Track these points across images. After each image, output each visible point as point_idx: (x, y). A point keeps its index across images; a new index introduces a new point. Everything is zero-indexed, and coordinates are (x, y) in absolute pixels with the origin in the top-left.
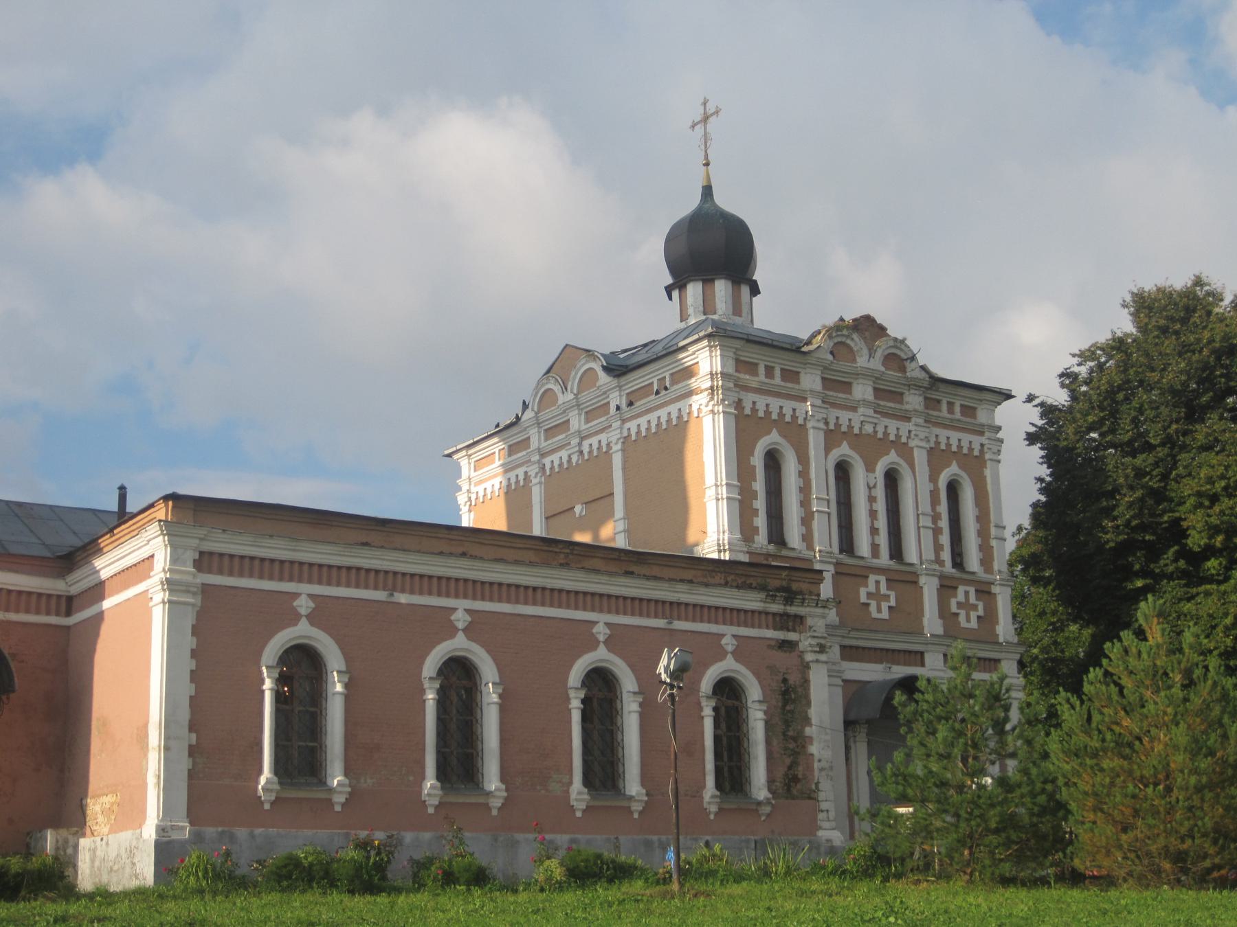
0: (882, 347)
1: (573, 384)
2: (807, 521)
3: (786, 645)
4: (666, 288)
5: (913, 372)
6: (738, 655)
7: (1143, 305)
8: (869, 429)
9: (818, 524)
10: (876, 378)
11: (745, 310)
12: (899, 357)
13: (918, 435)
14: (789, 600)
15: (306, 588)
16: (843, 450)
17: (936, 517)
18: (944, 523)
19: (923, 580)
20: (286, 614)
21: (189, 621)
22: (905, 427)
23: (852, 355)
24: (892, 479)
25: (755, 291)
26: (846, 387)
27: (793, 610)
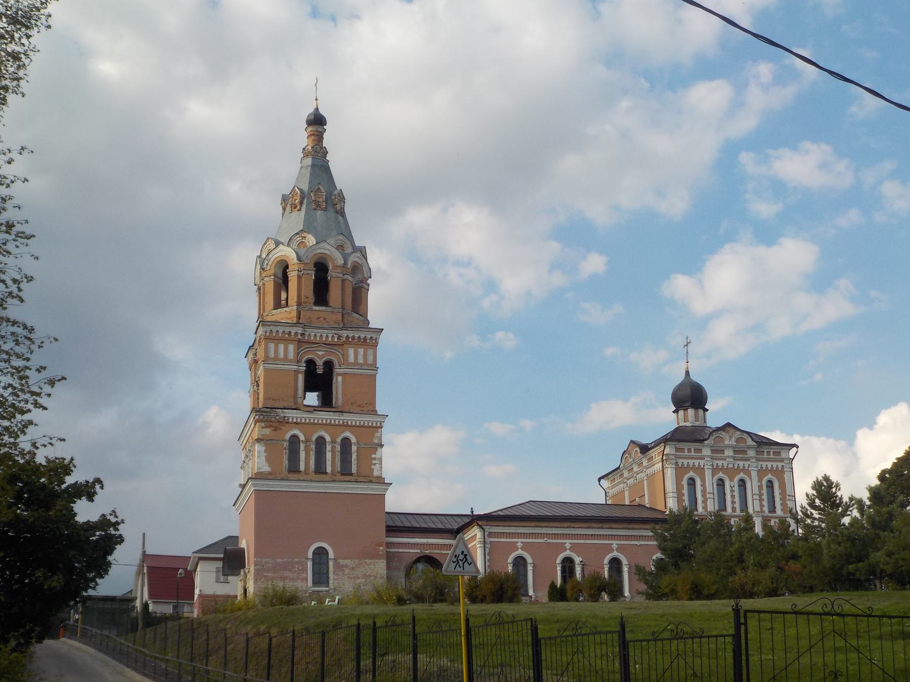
4: (632, 442)
8: (731, 466)
16: (720, 475)
17: (760, 495)
19: (755, 519)
20: (514, 547)
22: (747, 464)
23: (722, 440)
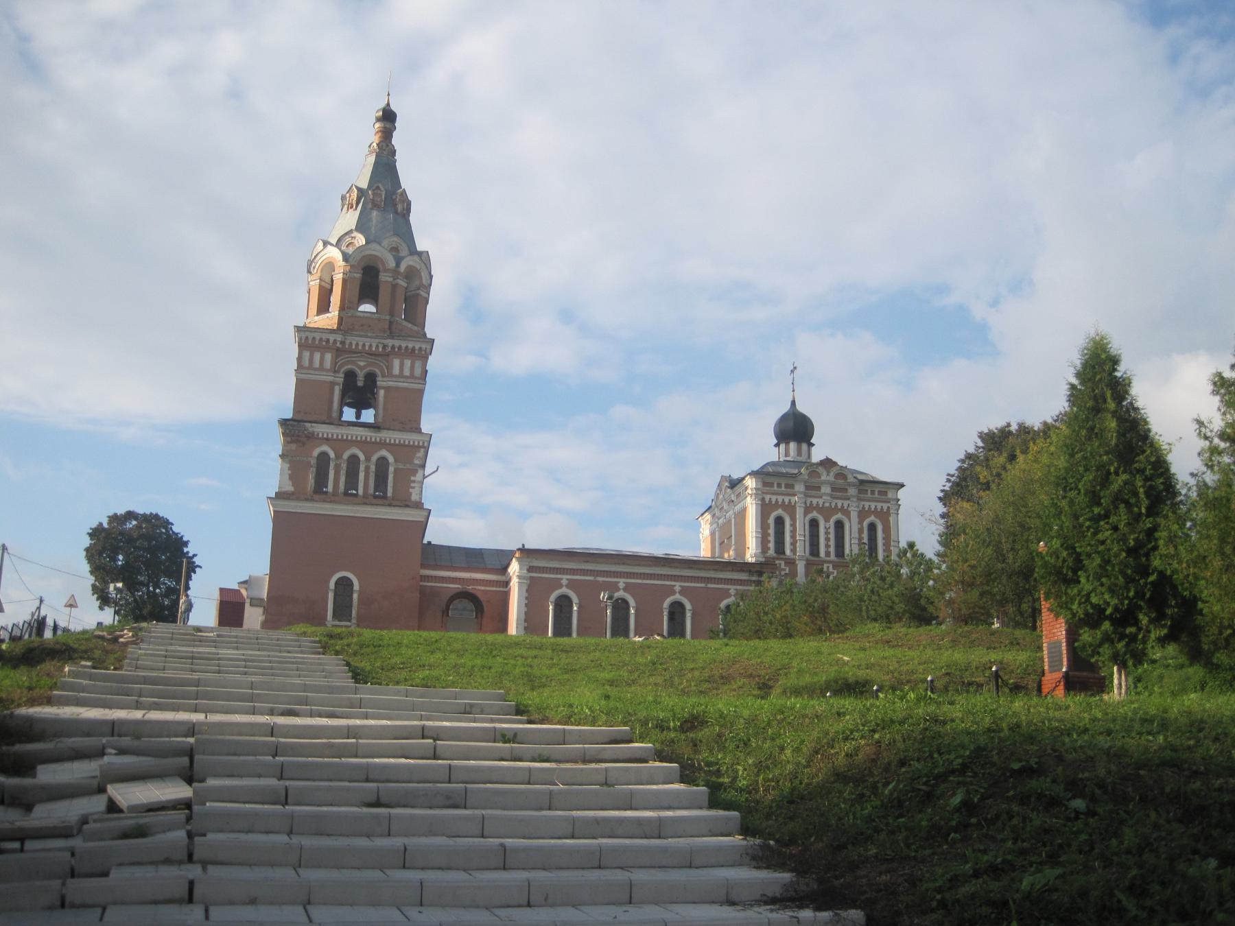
2: (794, 544)
5: (851, 479)
7: (982, 436)
8: (827, 505)
12: (843, 473)
20: (557, 584)
21: (525, 588)
22: (846, 503)
23: (819, 476)
24: (839, 526)
26: (818, 488)
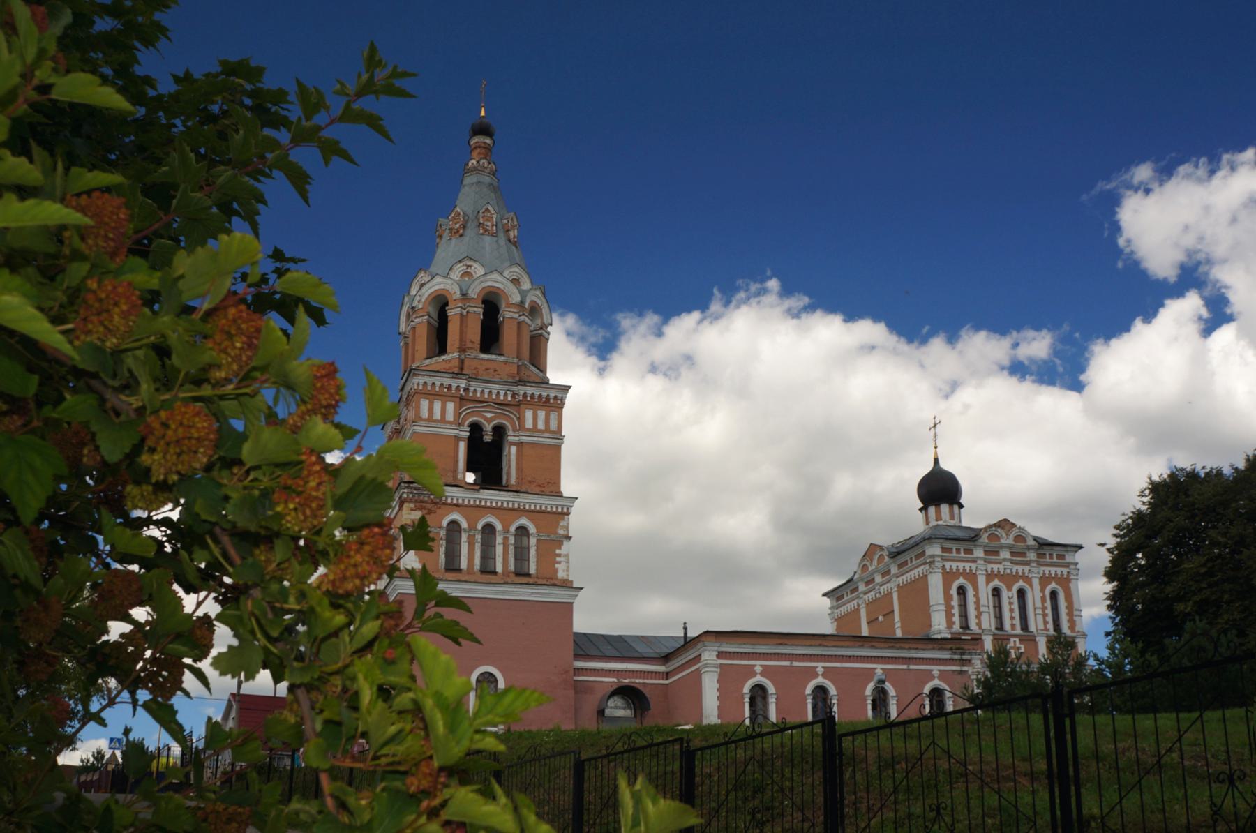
0: (1014, 532)
1: (875, 562)
2: (979, 616)
3: (961, 672)
6: (940, 678)
9: (985, 618)
10: (1010, 547)
11: (956, 516)
13: (1035, 573)
14: (963, 654)
15: (820, 665)
16: (996, 582)
17: (1044, 609)
18: (1049, 611)
24: (1021, 594)
25: (961, 506)
27: (965, 657)
